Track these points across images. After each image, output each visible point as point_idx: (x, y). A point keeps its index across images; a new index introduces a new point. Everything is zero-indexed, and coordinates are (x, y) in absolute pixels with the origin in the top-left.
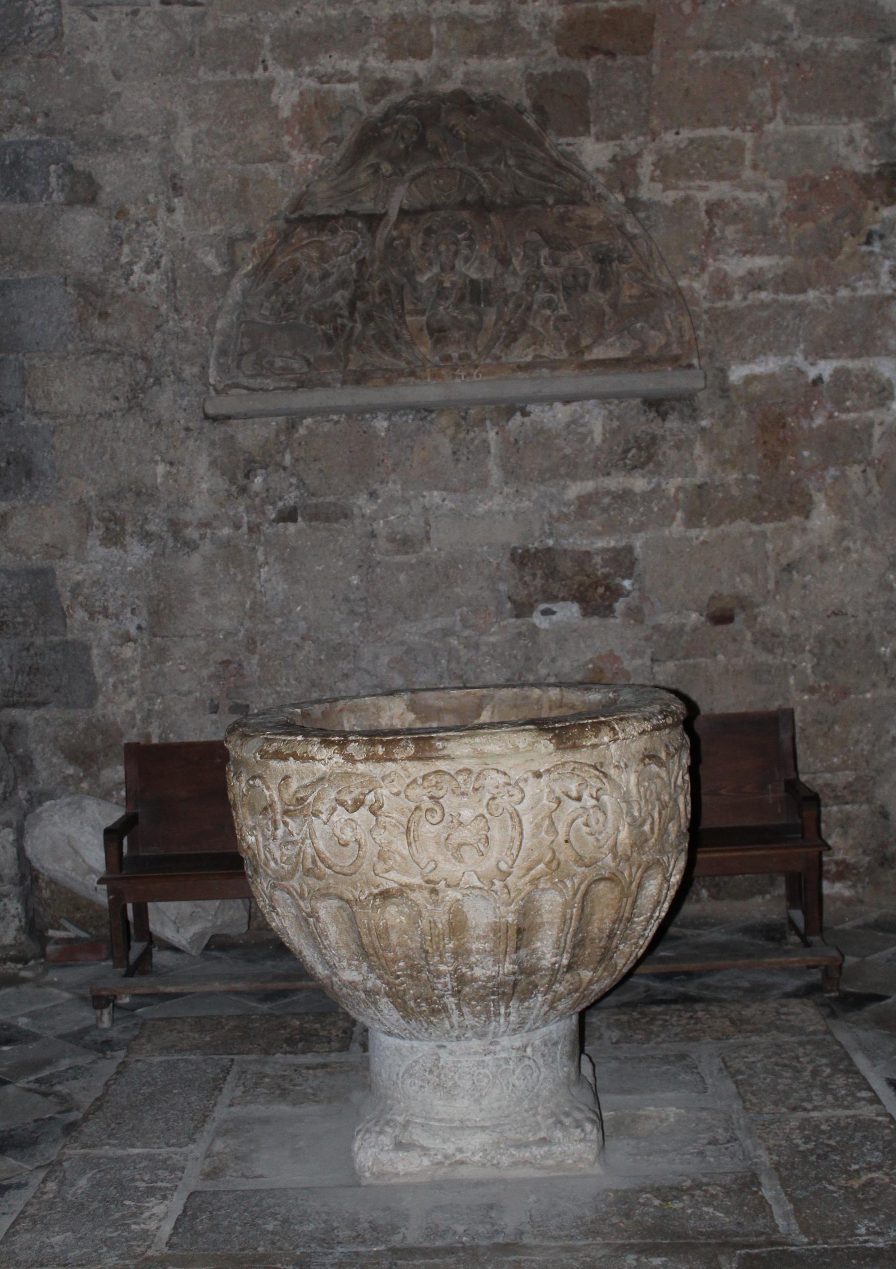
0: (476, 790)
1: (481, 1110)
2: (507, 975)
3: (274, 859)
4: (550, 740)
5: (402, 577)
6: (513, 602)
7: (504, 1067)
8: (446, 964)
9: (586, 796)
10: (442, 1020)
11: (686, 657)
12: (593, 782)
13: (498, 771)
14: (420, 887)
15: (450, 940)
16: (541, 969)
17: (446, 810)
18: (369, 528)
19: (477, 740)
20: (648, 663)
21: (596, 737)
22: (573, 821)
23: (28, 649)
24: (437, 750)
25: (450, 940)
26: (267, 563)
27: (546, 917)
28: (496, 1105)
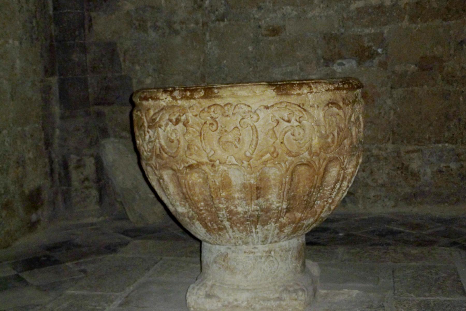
0: (234, 114)
1: (247, 281)
2: (254, 211)
3: (145, 151)
4: (274, 90)
5: (272, 47)
6: (324, 59)
7: (260, 260)
8: (222, 204)
9: (293, 120)
10: (225, 233)
11: (408, 86)
12: (298, 114)
13: (245, 105)
14: (207, 163)
15: (223, 191)
16: (272, 210)
17: (219, 125)
18: (257, 24)
19: (235, 88)
20: (389, 89)
21: (300, 90)
22: (286, 133)
23: (105, 79)
24: (215, 93)
25: (223, 191)
26: (210, 41)
27: (272, 182)
28: (255, 279)
